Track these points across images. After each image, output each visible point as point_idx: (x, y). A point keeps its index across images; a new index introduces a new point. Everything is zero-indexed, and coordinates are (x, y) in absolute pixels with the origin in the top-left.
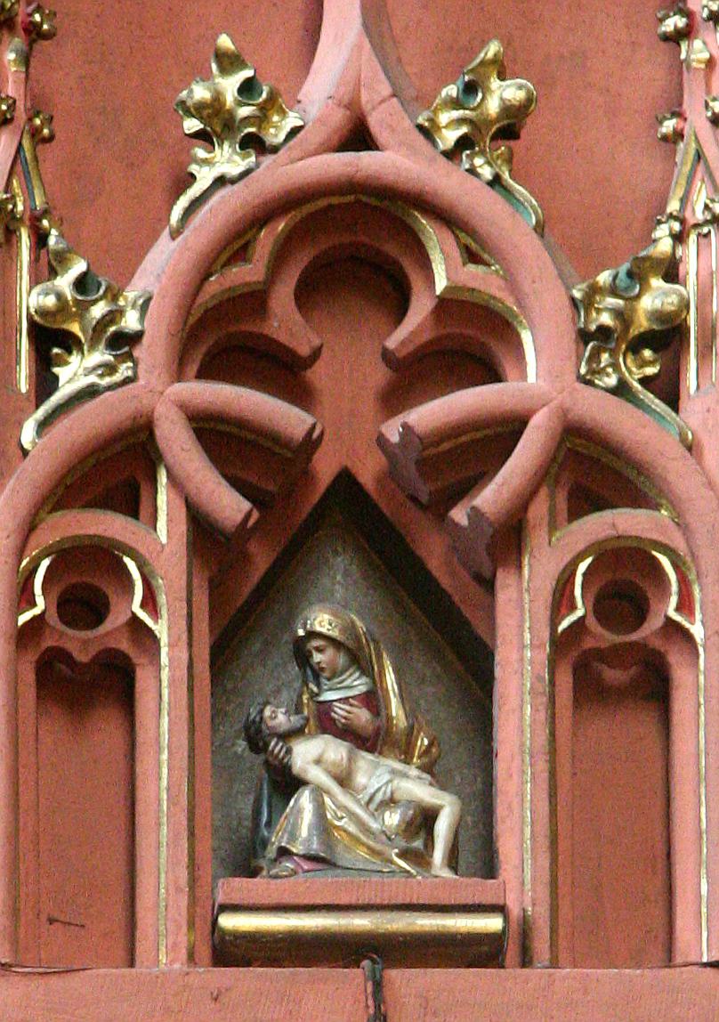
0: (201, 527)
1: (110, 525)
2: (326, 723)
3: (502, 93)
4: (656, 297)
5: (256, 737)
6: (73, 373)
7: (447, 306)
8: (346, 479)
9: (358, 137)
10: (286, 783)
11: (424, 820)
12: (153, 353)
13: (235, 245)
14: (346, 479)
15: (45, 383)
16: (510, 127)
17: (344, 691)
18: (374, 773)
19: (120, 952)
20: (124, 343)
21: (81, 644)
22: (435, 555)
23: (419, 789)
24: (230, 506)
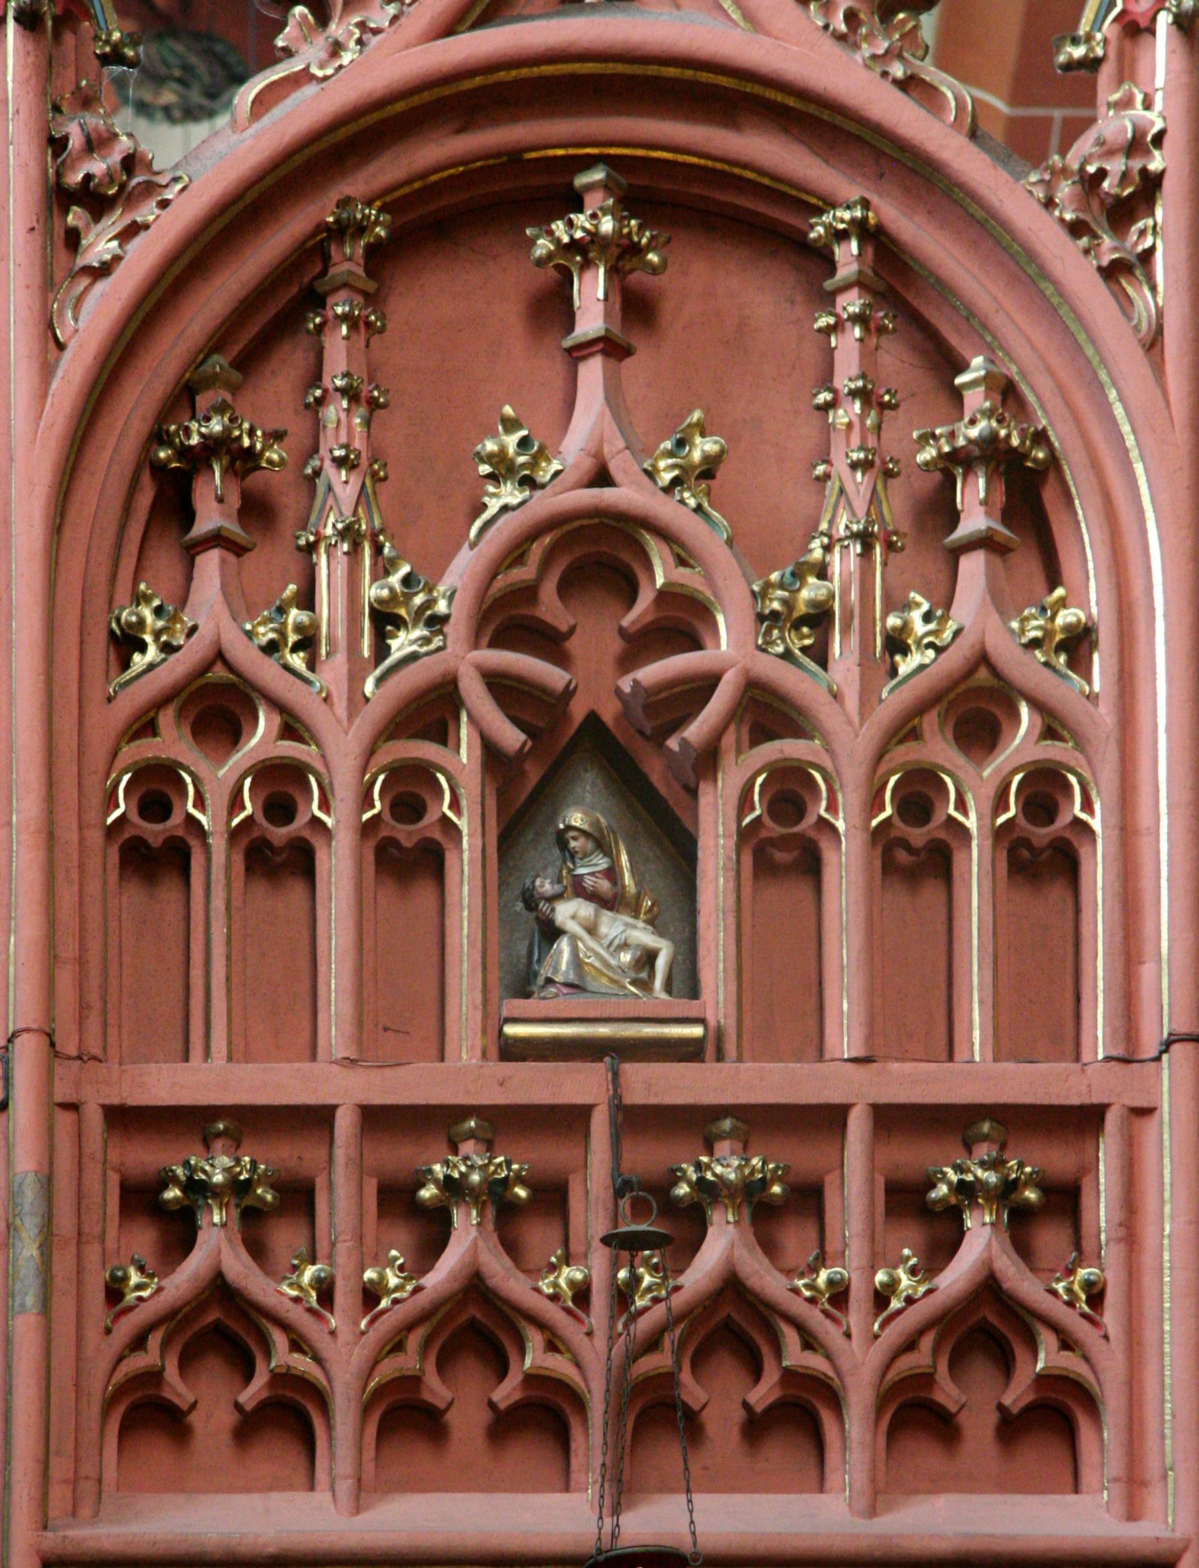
0: (491, 752)
1: (427, 750)
2: (579, 890)
3: (703, 447)
4: (811, 591)
5: (530, 900)
6: (401, 643)
7: (664, 596)
8: (593, 718)
9: (602, 477)
10: (551, 932)
11: (648, 958)
12: (458, 629)
13: (515, 554)
14: (593, 718)
15: (381, 651)
16: (709, 470)
17: (591, 868)
18: (613, 926)
19: (435, 1052)
20: (437, 622)
21: (406, 834)
22: (655, 772)
23: (644, 936)
24: (511, 737)
